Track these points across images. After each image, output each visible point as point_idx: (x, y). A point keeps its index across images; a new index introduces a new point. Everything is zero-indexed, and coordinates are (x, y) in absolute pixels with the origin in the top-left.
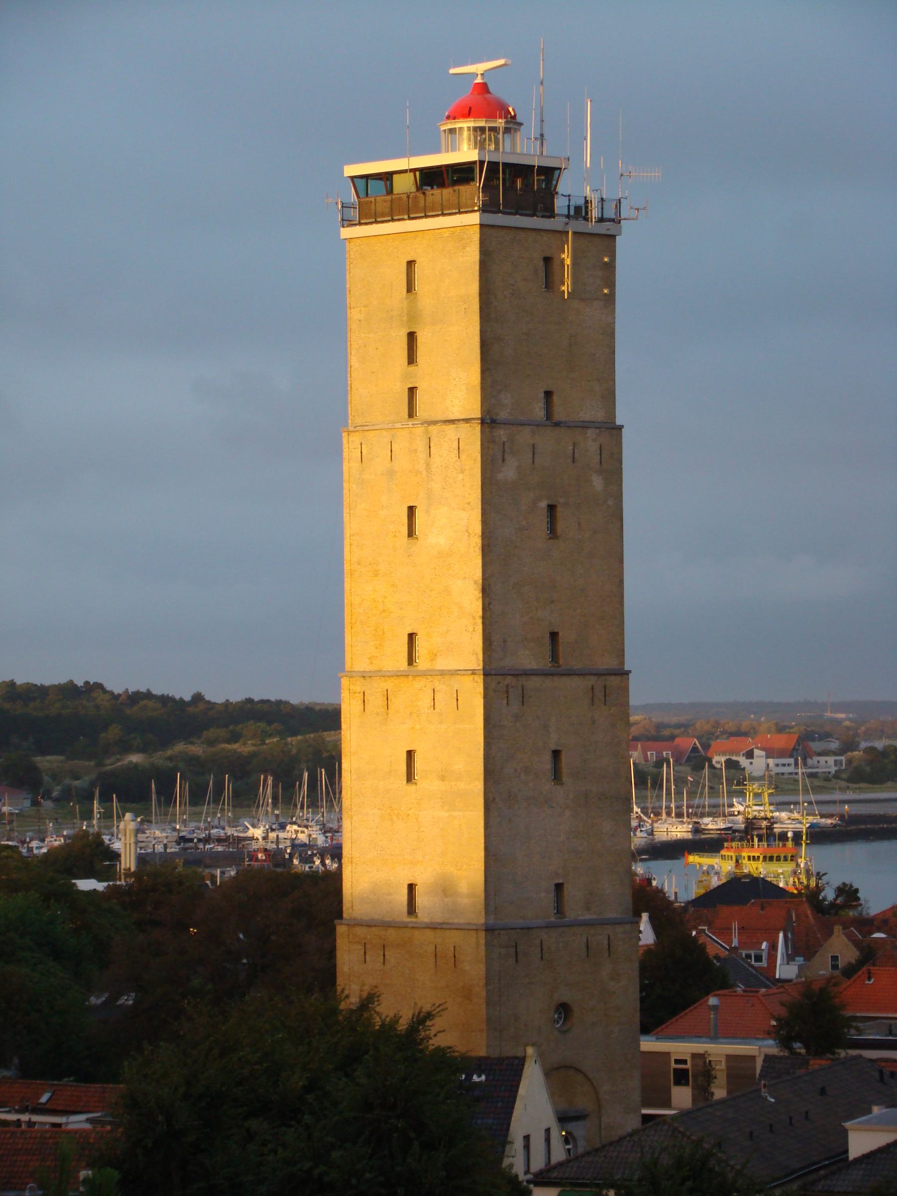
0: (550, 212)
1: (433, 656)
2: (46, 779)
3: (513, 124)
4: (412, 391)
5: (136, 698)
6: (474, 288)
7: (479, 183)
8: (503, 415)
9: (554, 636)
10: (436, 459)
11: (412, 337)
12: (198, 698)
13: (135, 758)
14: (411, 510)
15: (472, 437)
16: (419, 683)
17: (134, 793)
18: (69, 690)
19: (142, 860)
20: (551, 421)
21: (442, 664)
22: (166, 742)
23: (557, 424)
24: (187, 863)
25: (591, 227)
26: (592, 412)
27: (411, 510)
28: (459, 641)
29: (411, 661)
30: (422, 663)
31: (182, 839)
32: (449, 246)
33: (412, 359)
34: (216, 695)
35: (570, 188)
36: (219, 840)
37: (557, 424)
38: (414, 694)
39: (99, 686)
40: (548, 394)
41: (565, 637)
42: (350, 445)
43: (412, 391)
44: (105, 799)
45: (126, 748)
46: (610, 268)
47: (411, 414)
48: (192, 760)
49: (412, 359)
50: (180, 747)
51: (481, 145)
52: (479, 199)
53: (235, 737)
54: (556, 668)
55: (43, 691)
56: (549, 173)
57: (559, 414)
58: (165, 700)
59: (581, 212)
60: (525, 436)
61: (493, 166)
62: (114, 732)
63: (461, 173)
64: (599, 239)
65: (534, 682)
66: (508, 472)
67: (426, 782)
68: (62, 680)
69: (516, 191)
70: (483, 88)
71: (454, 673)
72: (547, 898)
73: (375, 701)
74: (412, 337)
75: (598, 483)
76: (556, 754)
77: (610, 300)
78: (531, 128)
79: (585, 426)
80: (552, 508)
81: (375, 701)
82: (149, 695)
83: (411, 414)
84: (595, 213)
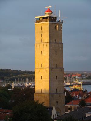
0: (56, 22)
1: (44, 66)
2: (5, 79)
3: (52, 13)
4: (42, 40)
5: (14, 71)
6: (48, 29)
7: (49, 19)
8: (51, 42)
9: (56, 64)
10: (44, 47)
11: (42, 34)
12: (20, 71)
13: (14, 77)
14: (42, 52)
15: (48, 44)
16: (42, 69)
17: (14, 80)
18: (7, 70)
19: (14, 87)
20: (56, 43)
21: (45, 67)
22: (17, 75)
23: (56, 43)
24: (19, 87)
25: (60, 23)
26: (60, 42)
27: (42, 52)
28: (47, 65)
29: (42, 67)
30: (43, 67)
31: (19, 85)
32: (46, 25)
33: (42, 36)
34: (22, 70)
35: (58, 19)
36: (22, 85)
37: (56, 43)
38: (42, 70)
39: (10, 69)
40: (56, 40)
41: (57, 64)
42: (36, 45)
43: (42, 40)
44: (11, 81)
45: (13, 76)
46: (62, 27)
47: (42, 42)
48: (20, 77)
49: (42, 36)
50: (18, 76)
51: (49, 15)
52: (49, 20)
53: (24, 75)
54: (56, 68)
55: (4, 70)
56: (56, 18)
57: (57, 42)
58: (17, 71)
59: (59, 22)
60: (53, 44)
61: (50, 17)
62: (12, 74)
63: (47, 18)
64: (61, 24)
65: (54, 69)
66: (52, 48)
67: (43, 79)
68: (6, 69)
69: (52, 19)
70: (49, 9)
71: (46, 68)
72: (56, 91)
73: (38, 71)
74: (42, 34)
75: (61, 49)
76: (56, 76)
77: (62, 30)
78: (54, 13)
79: (59, 43)
80: (56, 51)
81: (38, 71)
82: (15, 70)
83: (42, 42)
84: (60, 22)
